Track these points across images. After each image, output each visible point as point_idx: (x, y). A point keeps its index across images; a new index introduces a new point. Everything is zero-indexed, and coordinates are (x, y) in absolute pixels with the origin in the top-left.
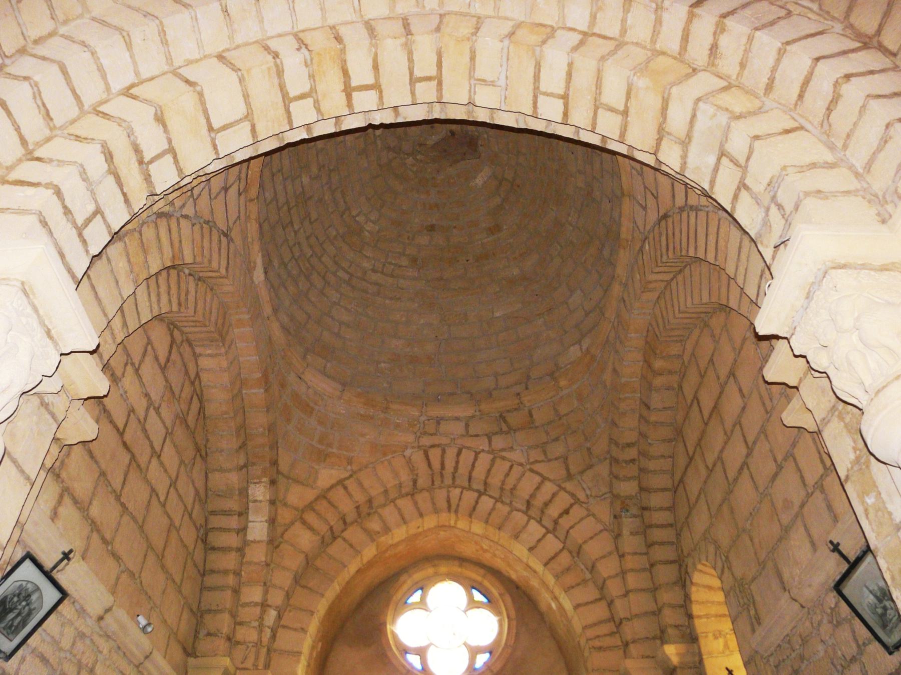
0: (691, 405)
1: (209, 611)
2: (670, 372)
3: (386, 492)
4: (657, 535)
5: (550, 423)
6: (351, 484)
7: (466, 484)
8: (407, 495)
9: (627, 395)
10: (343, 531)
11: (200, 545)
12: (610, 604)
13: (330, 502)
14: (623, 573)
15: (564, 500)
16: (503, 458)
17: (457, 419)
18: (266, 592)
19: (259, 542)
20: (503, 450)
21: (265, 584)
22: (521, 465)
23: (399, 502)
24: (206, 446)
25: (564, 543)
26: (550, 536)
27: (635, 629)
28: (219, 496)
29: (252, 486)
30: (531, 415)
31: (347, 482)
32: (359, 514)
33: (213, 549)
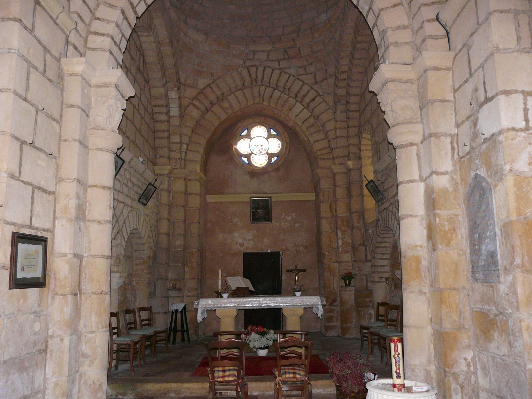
0: (371, 61)
1: (159, 147)
2: (365, 42)
3: (230, 89)
4: (351, 115)
5: (308, 55)
6: (214, 86)
7: (268, 84)
8: (240, 90)
9: (344, 49)
10: (211, 108)
11: (152, 121)
12: (329, 141)
13: (205, 95)
14: (336, 129)
15: (313, 94)
16: (285, 73)
17: (263, 51)
18: (181, 137)
19: (175, 116)
21: (180, 134)
22: (294, 76)
23: (236, 93)
24: (148, 77)
25: (312, 113)
26: (305, 110)
27: (338, 152)
28: (156, 98)
29: (170, 92)
30: (300, 51)
31: (212, 85)
32: (218, 100)
33: (157, 121)
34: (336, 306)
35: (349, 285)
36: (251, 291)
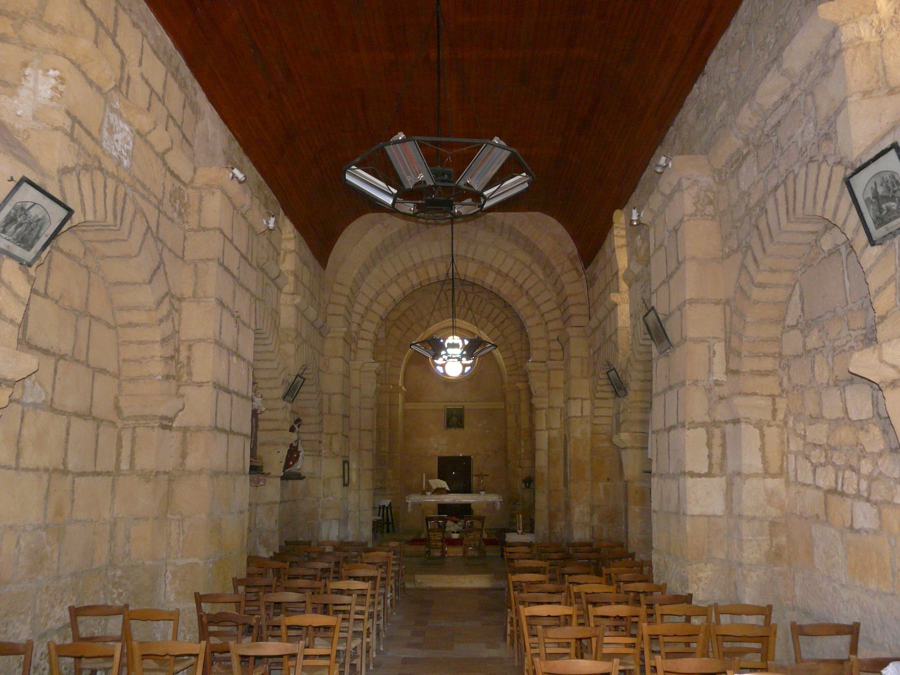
4: (548, 317)
16: (478, 296)
20: (479, 292)
26: (496, 329)
34: (519, 505)
35: (529, 487)
36: (446, 490)
